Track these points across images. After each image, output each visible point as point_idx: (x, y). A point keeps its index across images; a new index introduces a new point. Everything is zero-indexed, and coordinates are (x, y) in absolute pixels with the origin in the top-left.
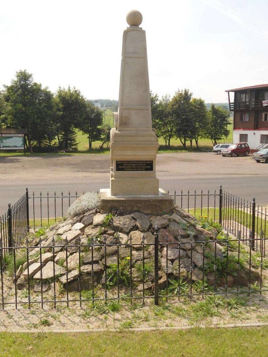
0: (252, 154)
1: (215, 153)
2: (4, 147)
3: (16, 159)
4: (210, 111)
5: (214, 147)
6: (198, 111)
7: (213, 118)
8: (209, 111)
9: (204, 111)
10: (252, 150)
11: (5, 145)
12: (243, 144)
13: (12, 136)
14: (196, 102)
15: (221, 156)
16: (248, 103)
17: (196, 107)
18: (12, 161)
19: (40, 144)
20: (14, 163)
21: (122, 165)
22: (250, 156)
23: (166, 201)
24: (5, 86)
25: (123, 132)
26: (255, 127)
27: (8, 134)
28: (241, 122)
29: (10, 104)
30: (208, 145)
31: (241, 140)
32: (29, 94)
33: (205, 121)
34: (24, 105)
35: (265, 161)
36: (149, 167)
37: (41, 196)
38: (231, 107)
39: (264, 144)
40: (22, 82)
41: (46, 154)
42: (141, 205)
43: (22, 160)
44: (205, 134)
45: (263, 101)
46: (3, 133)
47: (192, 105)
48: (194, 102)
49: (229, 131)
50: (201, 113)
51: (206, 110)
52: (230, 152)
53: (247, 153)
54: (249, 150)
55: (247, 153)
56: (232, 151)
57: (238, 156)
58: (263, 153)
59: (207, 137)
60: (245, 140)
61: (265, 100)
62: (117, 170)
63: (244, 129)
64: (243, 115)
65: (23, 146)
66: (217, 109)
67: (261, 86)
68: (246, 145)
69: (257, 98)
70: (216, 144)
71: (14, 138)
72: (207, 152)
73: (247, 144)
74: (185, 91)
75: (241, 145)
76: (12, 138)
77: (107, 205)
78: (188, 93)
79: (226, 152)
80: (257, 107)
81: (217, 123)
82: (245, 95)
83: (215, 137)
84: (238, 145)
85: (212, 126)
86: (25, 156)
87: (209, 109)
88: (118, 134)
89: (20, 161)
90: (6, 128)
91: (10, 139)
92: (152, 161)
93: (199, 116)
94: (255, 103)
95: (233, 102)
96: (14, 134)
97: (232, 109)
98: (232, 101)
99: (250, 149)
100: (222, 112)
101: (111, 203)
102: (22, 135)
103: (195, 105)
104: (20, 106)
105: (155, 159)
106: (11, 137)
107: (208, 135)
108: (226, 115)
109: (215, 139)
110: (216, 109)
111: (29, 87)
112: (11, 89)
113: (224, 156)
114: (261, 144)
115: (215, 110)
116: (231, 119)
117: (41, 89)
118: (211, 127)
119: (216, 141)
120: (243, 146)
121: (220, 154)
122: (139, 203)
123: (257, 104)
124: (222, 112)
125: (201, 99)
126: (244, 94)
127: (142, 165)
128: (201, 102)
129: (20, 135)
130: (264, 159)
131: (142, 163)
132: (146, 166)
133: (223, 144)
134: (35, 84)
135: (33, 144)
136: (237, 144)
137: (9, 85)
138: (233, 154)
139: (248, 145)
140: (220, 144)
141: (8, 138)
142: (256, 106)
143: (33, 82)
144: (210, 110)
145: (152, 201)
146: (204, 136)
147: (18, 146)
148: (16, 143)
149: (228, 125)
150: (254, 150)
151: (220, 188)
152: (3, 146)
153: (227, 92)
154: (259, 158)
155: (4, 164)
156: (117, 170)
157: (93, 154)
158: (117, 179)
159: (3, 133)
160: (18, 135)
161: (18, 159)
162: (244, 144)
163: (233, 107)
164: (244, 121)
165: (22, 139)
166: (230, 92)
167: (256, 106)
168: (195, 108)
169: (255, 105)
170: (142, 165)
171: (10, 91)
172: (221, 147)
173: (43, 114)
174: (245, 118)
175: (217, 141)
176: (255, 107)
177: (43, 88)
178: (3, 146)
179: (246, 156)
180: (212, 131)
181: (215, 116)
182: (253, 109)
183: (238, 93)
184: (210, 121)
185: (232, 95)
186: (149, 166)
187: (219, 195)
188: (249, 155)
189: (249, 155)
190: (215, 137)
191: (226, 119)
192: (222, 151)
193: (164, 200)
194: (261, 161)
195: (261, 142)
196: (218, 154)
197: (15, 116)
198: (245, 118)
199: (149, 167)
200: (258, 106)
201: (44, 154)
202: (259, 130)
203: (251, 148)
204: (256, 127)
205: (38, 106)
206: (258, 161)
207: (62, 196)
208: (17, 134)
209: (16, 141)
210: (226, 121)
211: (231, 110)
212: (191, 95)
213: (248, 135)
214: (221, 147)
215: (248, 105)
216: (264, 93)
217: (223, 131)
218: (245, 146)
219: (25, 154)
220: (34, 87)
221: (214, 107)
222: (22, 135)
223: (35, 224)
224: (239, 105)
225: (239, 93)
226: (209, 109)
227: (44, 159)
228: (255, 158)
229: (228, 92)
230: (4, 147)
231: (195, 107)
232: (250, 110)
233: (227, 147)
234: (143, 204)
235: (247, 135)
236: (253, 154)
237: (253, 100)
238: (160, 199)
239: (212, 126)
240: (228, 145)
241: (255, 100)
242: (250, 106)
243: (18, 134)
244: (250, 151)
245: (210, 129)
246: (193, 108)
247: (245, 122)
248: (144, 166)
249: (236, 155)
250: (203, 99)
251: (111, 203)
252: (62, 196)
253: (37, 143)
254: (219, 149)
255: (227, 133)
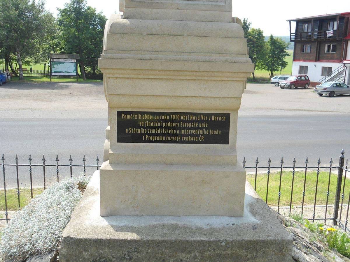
0: (315, 87)
1: (272, 84)
2: (55, 72)
3: (66, 86)
4: (269, 42)
5: (272, 79)
6: (256, 41)
7: (271, 48)
8: (267, 42)
9: (263, 41)
10: (311, 82)
11: (56, 71)
12: (303, 76)
13: (64, 61)
14: (255, 32)
15: (279, 87)
16: (310, 34)
17: (255, 37)
18: (61, 88)
19: (94, 71)
20: (63, 89)
21: (134, 124)
22: (309, 89)
23: (265, 244)
24: (58, 9)
25: (134, 21)
26: (316, 58)
27: (60, 59)
28: (301, 53)
29: (63, 28)
30: (264, 76)
31: (300, 72)
32: (82, 18)
33: (263, 52)
34: (78, 30)
35: (328, 95)
36: (218, 132)
37: (3, 161)
38: (292, 37)
39: (326, 77)
40: (76, 5)
41: (100, 80)
42: (189, 256)
43: (72, 87)
44: (262, 65)
45: (327, 32)
46: (54, 58)
47: (250, 35)
48: (253, 32)
49: (287, 62)
50: (259, 43)
51: (265, 41)
52: (289, 84)
53: (307, 86)
54: (309, 82)
55: (307, 86)
56: (291, 83)
57: (297, 88)
58: (327, 87)
59: (264, 68)
60: (305, 71)
61: (329, 30)
62: (119, 140)
63: (305, 60)
64: (303, 46)
65: (75, 72)
66: (276, 39)
67: (324, 16)
68: (306, 77)
69: (320, 28)
70: (273, 76)
71: (65, 63)
72: (264, 83)
73: (307, 76)
74: (244, 20)
75: (301, 77)
76: (63, 63)
77: (81, 253)
78: (247, 22)
79: (284, 84)
80: (320, 38)
81: (275, 54)
82: (308, 25)
83: (272, 68)
84: (298, 77)
85: (269, 57)
86: (77, 82)
87: (267, 40)
88: (123, 26)
89: (68, 88)
90: (60, 53)
91: (62, 64)
92: (228, 116)
93: (258, 46)
94: (318, 33)
95: (294, 32)
96: (65, 59)
97: (292, 39)
98: (293, 30)
99: (310, 81)
100: (281, 43)
101: (93, 250)
102: (75, 61)
103: (253, 35)
104: (73, 30)
105: (236, 110)
106: (63, 63)
107: (265, 66)
108: (285, 46)
109: (272, 71)
110: (274, 39)
111: (83, 10)
112: (64, 12)
113: (282, 88)
114: (323, 77)
115: (273, 41)
116: (290, 51)
117: (96, 13)
118: (269, 58)
119: (273, 72)
120: (303, 78)
121: (278, 86)
122: (184, 250)
123: (320, 34)
124: (281, 43)
125: (260, 29)
126: (307, 23)
127: (195, 125)
128: (260, 32)
129: (73, 61)
130: (327, 93)
131: (196, 121)
132: (206, 129)
133: (281, 76)
134: (89, 8)
135: (87, 70)
136: (296, 76)
137: (62, 8)
138: (293, 87)
139: (308, 78)
140: (278, 76)
141: (60, 63)
142: (320, 37)
143: (87, 5)
144: (268, 40)
145: (223, 244)
146: (261, 67)
147: (69, 72)
148: (69, 69)
149: (286, 57)
150: (317, 83)
151: (341, 156)
152: (54, 71)
153: (289, 22)
154: (322, 91)
155: (52, 90)
156: (119, 140)
157: (46, 90)
158: (118, 168)
159: (54, 58)
160: (70, 61)
161: (68, 86)
162: (304, 76)
163: (294, 37)
164: (304, 52)
165: (74, 64)
166: (291, 22)
167: (320, 37)
168: (254, 38)
169: (318, 35)
170: (195, 125)
171: (63, 14)
172: (279, 78)
173: (97, 39)
174: (306, 48)
175: (274, 72)
176: (318, 38)
177: (97, 12)
178: (54, 71)
179: (305, 88)
180: (269, 62)
181: (273, 47)
182: (315, 40)
183: (300, 22)
184: (268, 52)
185: (294, 24)
186: (215, 128)
187: (339, 168)
188: (309, 87)
189: (309, 87)
190: (272, 68)
191: (285, 50)
192: (280, 83)
193: (263, 242)
194: (323, 95)
195: (322, 75)
196: (275, 86)
197: (68, 42)
198: (306, 48)
199: (218, 132)
200: (321, 37)
201: (98, 80)
202: (321, 62)
203: (311, 80)
204: (317, 59)
205: (92, 31)
206: (321, 95)
207: (44, 163)
208: (69, 59)
209: (69, 67)
210: (284, 52)
211: (291, 41)
212: (249, 24)
213: (308, 67)
214: (279, 78)
215: (310, 36)
216: (328, 24)
217: (280, 62)
218: (305, 78)
219: (77, 81)
220: (88, 11)
221: (273, 38)
222: (75, 61)
223: (8, 204)
224: (301, 35)
225: (301, 23)
226: (267, 40)
227: (96, 86)
228: (317, 91)
229: (290, 21)
230: (55, 72)
231: (254, 37)
232: (313, 40)
233: (285, 78)
234: (197, 254)
235: (307, 67)
236: (316, 87)
237: (317, 30)
238: (248, 237)
239: (269, 57)
240: (287, 76)
241: (319, 30)
242: (312, 37)
243: (70, 59)
244: (310, 84)
245: (267, 61)
246: (252, 38)
247: (305, 53)
248: (201, 129)
249: (295, 88)
250: (262, 29)
251: (93, 250)
252: (44, 163)
253: (92, 69)
254: (277, 80)
255: (284, 64)
